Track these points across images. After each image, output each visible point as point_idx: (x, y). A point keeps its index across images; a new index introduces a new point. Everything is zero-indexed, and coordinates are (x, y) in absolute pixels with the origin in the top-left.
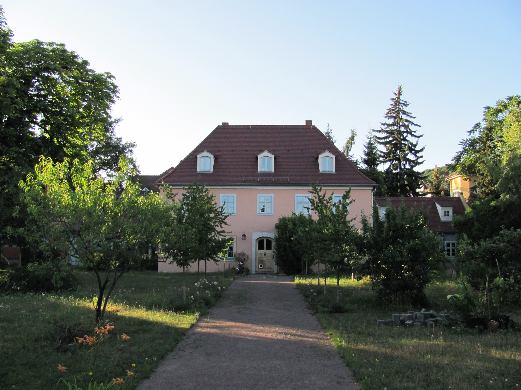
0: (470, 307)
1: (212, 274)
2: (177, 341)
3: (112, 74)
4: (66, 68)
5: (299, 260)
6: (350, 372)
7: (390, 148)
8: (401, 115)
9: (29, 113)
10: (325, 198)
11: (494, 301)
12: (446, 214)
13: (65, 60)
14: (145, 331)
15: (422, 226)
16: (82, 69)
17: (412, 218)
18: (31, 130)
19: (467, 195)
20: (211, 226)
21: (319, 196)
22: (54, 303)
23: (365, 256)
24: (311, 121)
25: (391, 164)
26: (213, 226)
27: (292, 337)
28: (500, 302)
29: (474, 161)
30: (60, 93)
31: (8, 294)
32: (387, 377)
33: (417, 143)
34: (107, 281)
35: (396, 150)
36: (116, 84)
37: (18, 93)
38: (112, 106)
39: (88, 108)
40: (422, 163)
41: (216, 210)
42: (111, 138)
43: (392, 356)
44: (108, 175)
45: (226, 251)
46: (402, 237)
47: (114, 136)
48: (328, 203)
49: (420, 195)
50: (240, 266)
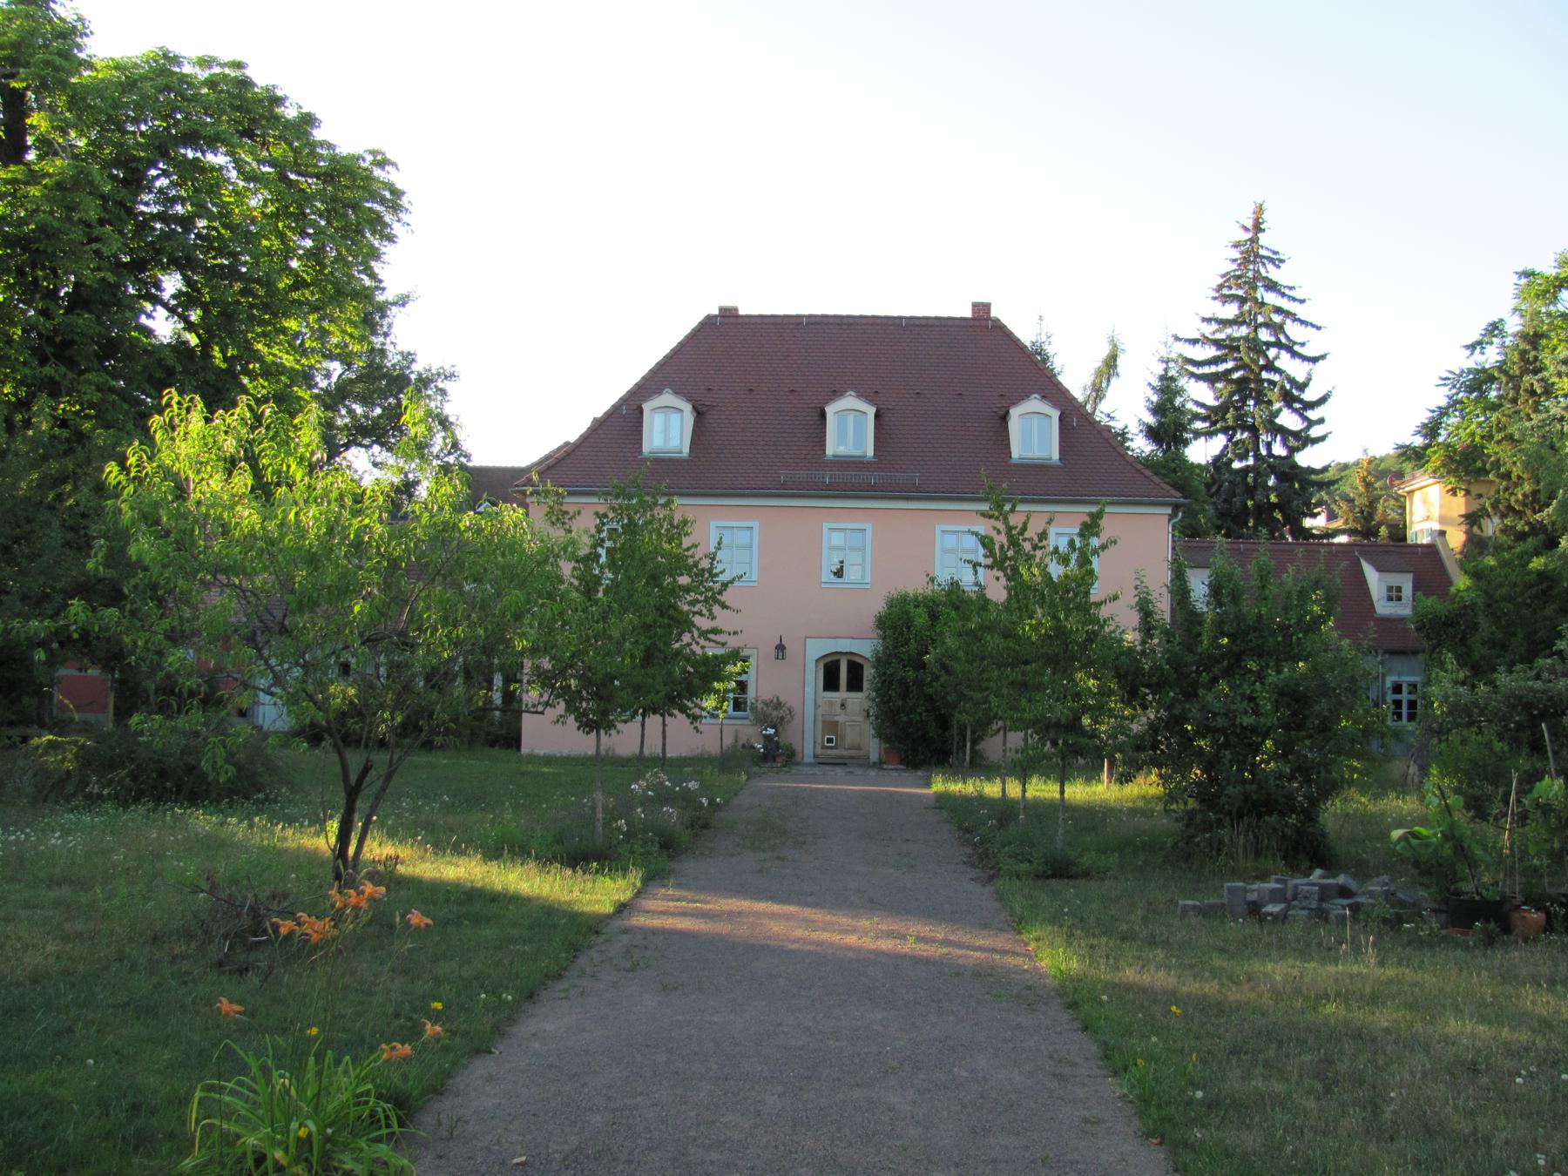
0: (1458, 867)
1: (682, 762)
2: (575, 949)
3: (389, 156)
4: (248, 133)
5: (944, 722)
6: (1094, 1048)
7: (1226, 394)
8: (1261, 293)
9: (138, 266)
10: (1027, 535)
11: (1532, 850)
12: (1394, 594)
13: (246, 111)
14: (478, 920)
15: (1318, 621)
16: (298, 139)
17: (1289, 596)
18: (143, 319)
19: (1456, 538)
20: (681, 612)
21: (1010, 529)
22: (208, 836)
23: (1144, 707)
24: (987, 306)
25: (1230, 440)
26: (687, 614)
27: (921, 945)
28: (1551, 854)
29: (1483, 437)
30: (230, 213)
31: (76, 807)
32: (1204, 1062)
33: (1309, 379)
34: (366, 770)
35: (1243, 400)
36: (399, 186)
37: (105, 209)
38: (387, 249)
39: (315, 255)
40: (1322, 439)
41: (696, 564)
42: (383, 352)
43: (1220, 1003)
44: (375, 465)
45: (726, 691)
46: (1259, 653)
47: (390, 348)
48: (1035, 548)
49: (1314, 536)
50: (767, 737)
